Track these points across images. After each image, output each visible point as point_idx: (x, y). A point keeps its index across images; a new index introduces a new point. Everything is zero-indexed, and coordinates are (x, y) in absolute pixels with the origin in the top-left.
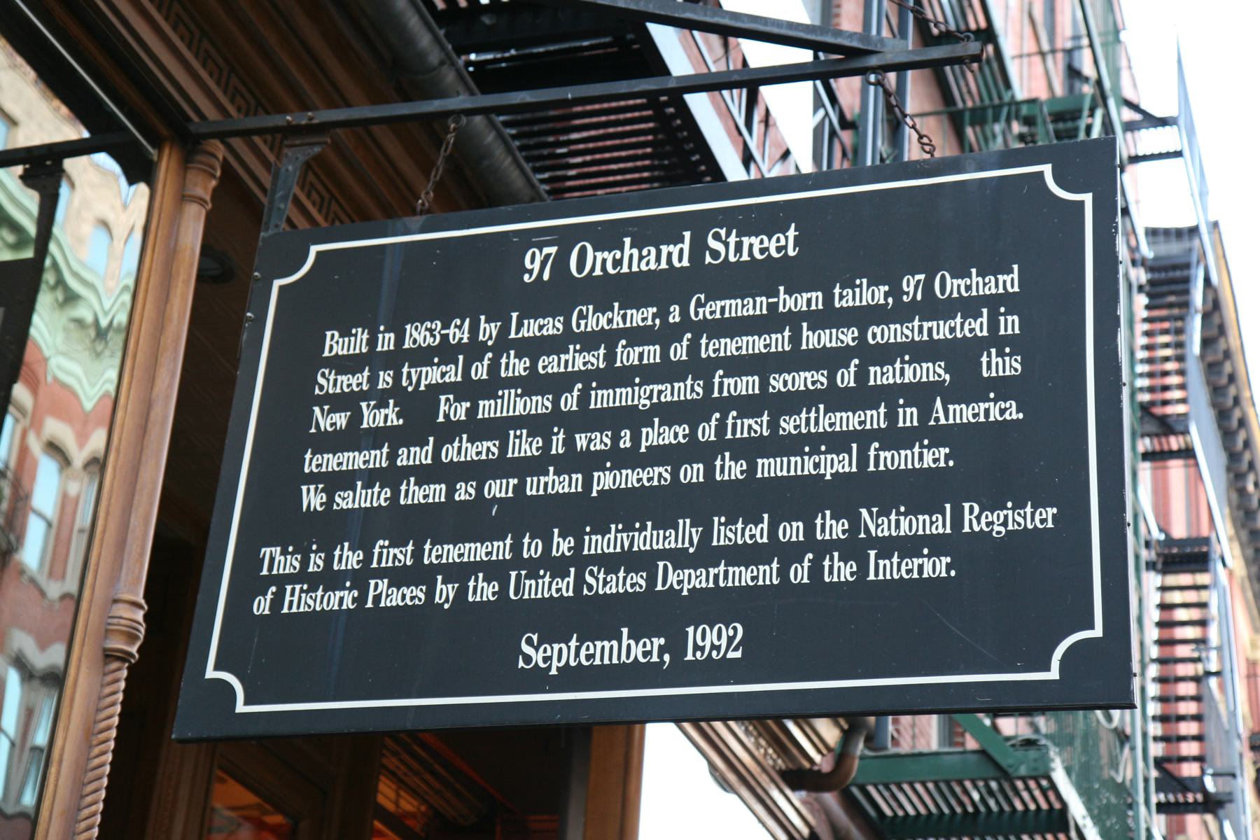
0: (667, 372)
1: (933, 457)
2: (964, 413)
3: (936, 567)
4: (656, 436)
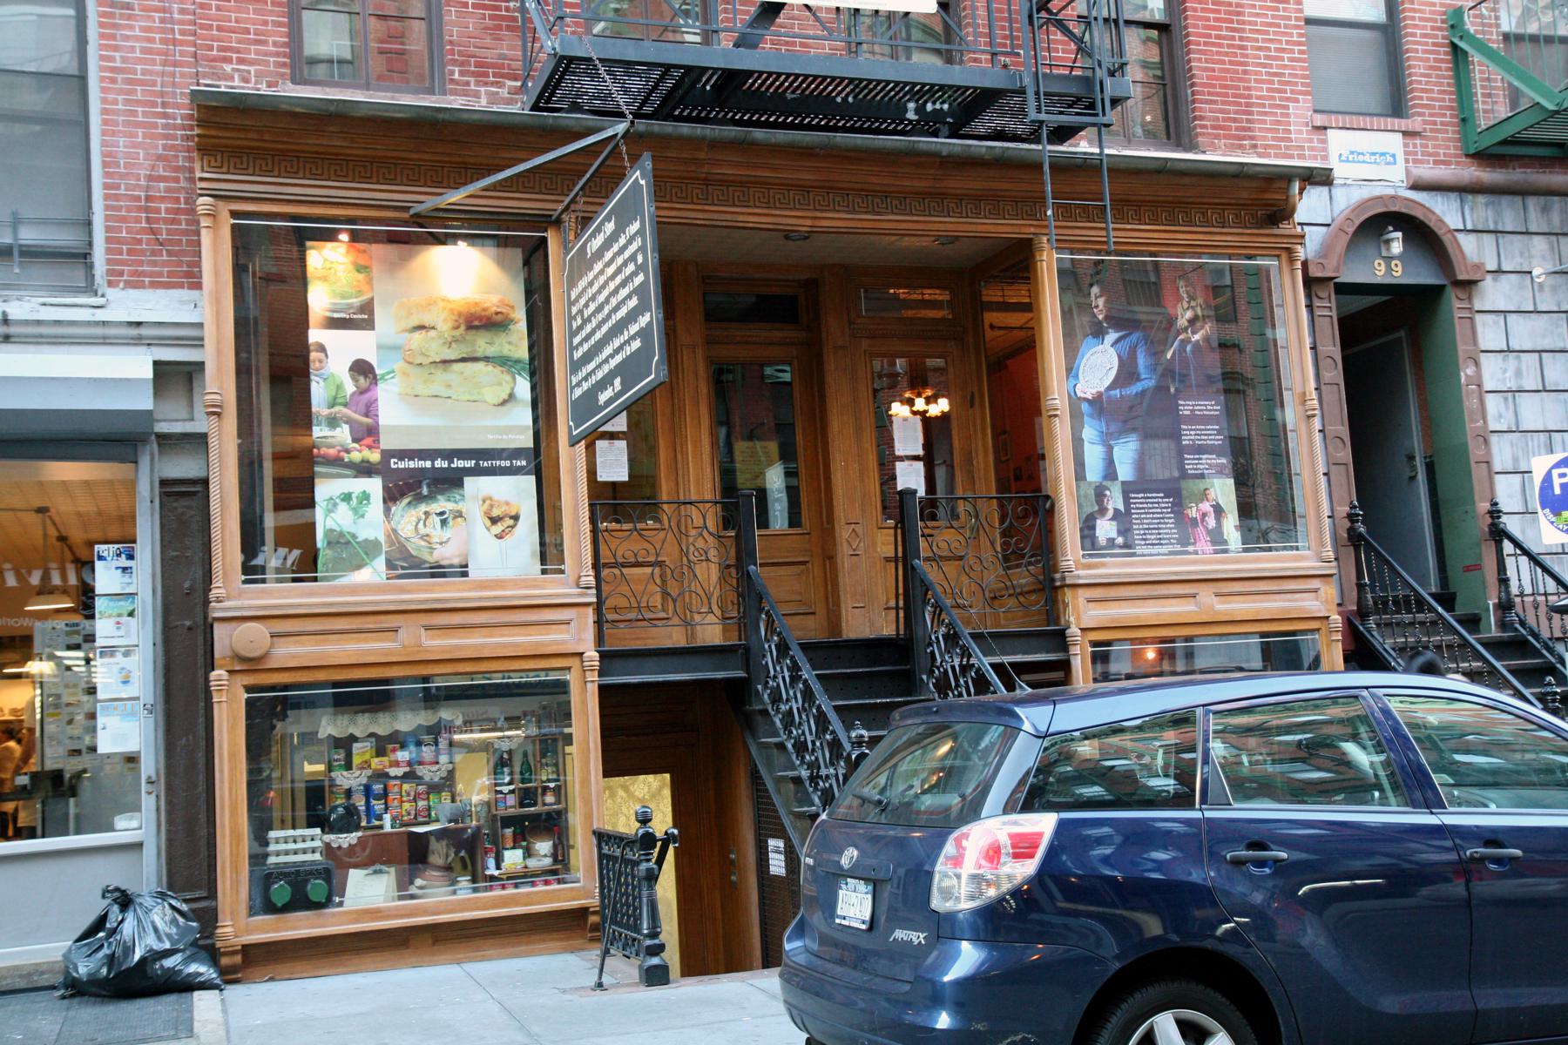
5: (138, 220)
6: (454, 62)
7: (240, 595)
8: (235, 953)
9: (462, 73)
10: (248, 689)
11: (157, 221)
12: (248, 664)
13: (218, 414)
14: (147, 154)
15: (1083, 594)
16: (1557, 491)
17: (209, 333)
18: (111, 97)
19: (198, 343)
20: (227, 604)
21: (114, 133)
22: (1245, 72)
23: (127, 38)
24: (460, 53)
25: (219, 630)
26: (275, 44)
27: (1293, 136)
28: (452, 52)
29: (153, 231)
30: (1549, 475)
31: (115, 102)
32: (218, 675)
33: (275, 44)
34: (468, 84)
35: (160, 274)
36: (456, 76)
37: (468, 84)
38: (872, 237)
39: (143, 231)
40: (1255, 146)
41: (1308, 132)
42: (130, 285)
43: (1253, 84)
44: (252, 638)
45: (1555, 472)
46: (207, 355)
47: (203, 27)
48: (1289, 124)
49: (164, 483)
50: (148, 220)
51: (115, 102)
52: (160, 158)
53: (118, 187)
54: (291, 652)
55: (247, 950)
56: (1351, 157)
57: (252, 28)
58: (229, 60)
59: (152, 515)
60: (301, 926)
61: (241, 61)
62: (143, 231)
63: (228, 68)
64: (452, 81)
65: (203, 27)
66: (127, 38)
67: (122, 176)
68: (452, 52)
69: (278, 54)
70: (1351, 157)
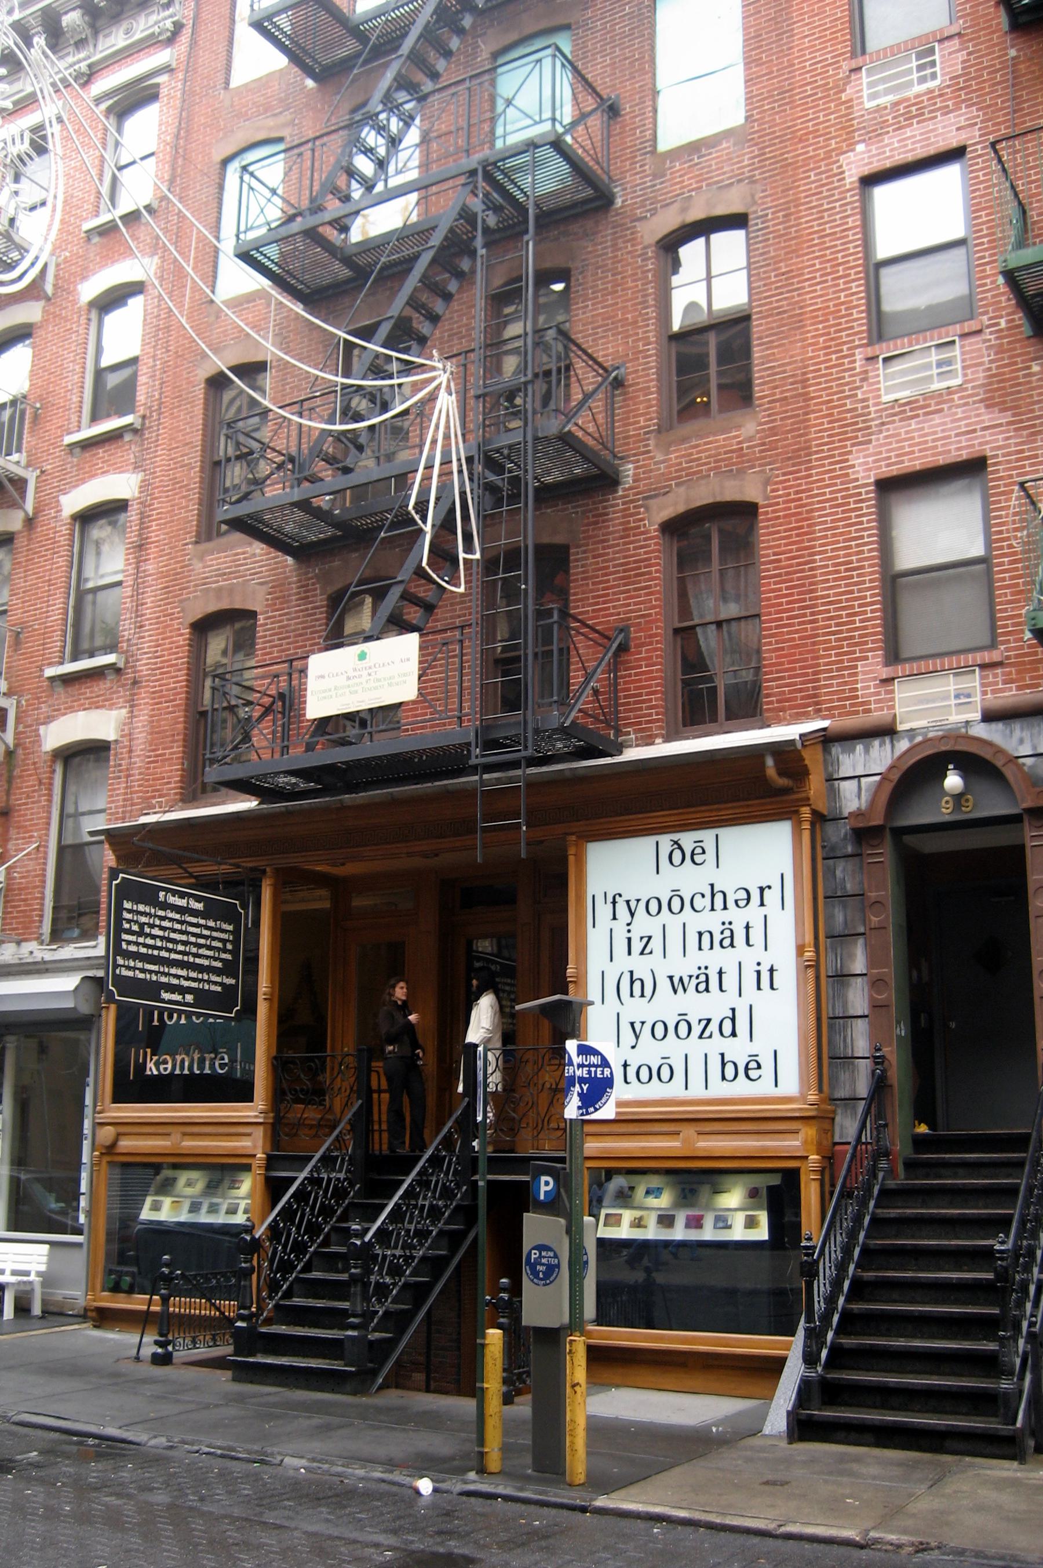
0: (181, 932)
1: (218, 964)
2: (224, 956)
3: (219, 989)
4: (181, 948)
40: (819, 710)
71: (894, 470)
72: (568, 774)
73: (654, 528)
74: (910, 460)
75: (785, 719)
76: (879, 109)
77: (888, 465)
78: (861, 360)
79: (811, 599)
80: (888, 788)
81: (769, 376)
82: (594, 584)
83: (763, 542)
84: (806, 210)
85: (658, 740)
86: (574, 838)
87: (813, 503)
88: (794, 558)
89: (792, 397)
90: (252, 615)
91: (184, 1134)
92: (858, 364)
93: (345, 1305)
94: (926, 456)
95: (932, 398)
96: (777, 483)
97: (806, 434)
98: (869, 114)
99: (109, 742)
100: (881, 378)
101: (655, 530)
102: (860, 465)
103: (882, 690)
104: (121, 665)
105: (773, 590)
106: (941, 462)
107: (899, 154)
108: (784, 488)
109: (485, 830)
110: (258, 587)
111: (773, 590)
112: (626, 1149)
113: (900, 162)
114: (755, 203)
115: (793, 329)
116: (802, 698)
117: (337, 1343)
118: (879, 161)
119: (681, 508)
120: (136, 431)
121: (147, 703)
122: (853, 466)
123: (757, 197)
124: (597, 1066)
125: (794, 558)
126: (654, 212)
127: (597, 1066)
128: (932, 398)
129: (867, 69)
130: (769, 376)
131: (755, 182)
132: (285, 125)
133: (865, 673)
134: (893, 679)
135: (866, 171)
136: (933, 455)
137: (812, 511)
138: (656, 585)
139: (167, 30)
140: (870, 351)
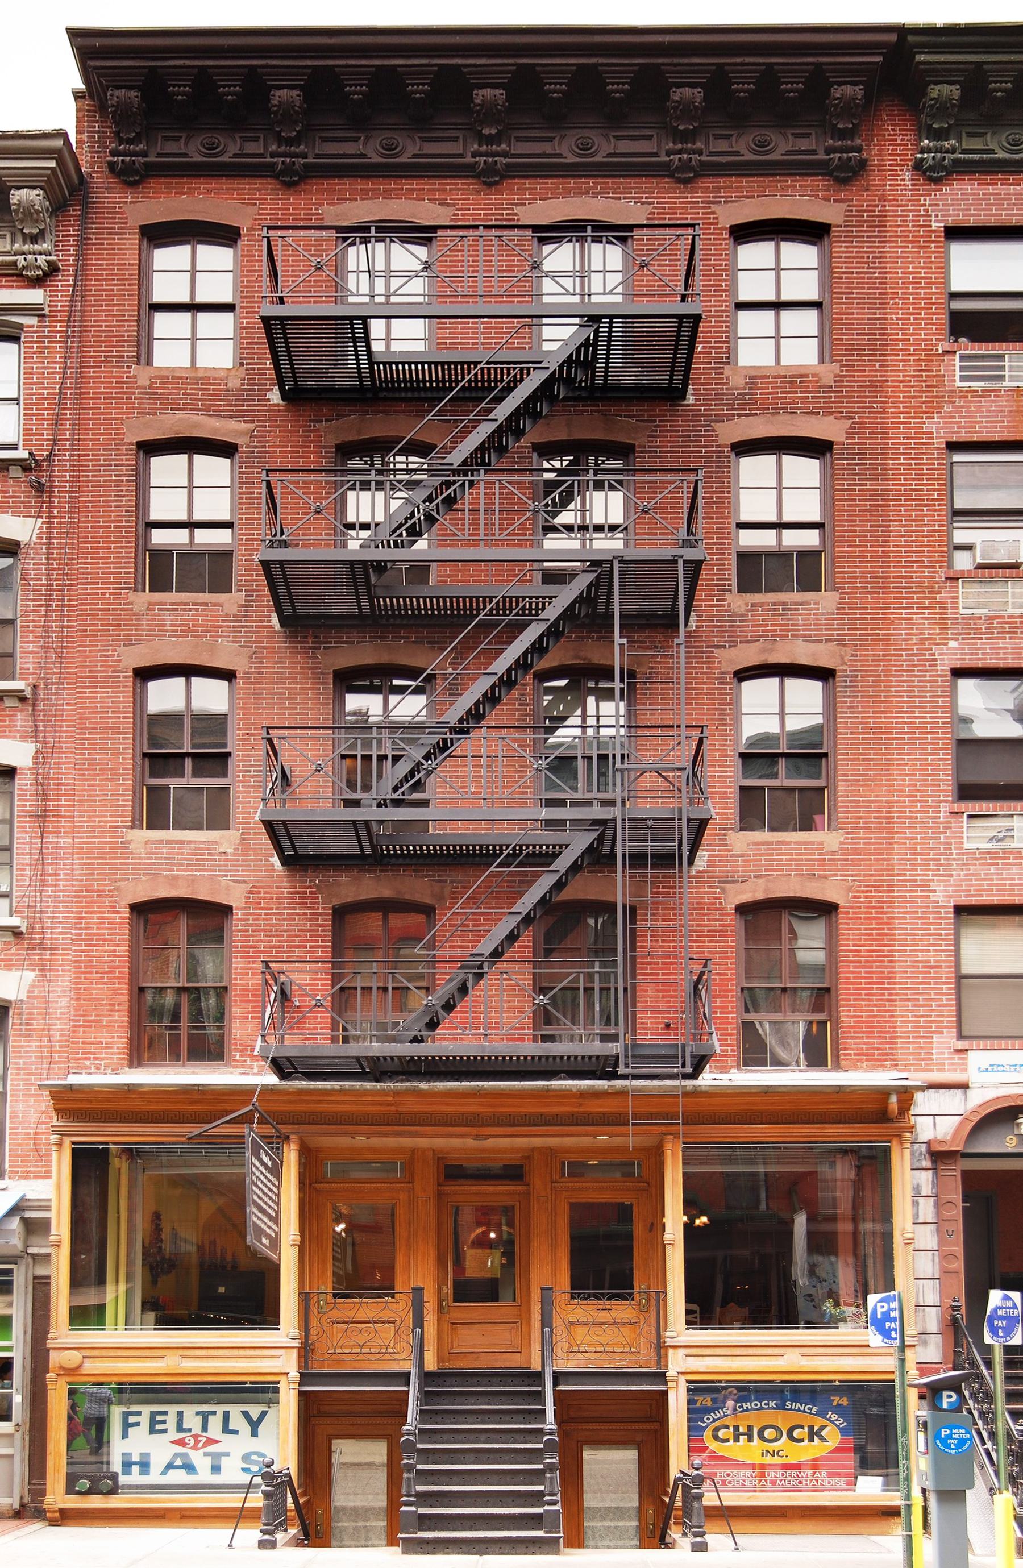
5: (28, 1145)
6: (237, 1050)
7: (67, 1336)
8: (55, 1512)
9: (241, 1056)
10: (70, 1383)
11: (40, 1144)
12: (72, 1371)
13: (58, 1246)
14: (35, 1112)
15: (682, 1352)
16: (879, 1316)
17: (54, 1204)
18: (15, 1082)
19: (48, 1208)
20: (59, 1341)
21: (17, 1101)
22: (892, 1016)
23: (27, 1052)
24: (241, 1045)
25: (53, 1355)
26: (118, 1048)
27: (934, 1057)
28: (236, 1044)
29: (37, 1150)
30: (876, 1306)
31: (19, 1085)
32: (50, 1376)
33: (118, 1048)
34: (245, 1061)
35: (40, 1172)
36: (237, 1058)
37: (245, 1061)
38: (645, 1127)
39: (32, 1150)
40: (896, 1065)
41: (949, 1053)
42: (21, 1178)
43: (899, 1024)
44: (72, 1358)
45: (879, 1305)
46: (52, 1215)
47: (73, 1042)
48: (932, 1048)
49: (35, 1278)
50: (35, 1144)
51: (19, 1085)
52: (43, 1112)
53: (17, 1128)
54: (89, 1367)
55: (62, 1511)
56: (990, 1069)
57: (104, 1040)
58: (88, 1059)
59: (26, 1294)
60: (96, 1502)
61: (96, 1059)
62: (32, 1150)
63: (87, 1063)
64: (234, 1060)
65: (73, 1042)
66: (27, 1052)
67: (20, 1123)
68: (236, 1044)
69: (120, 1053)
70: (990, 1069)
71: (974, 901)
72: (574, 1090)
73: (730, 907)
74: (988, 896)
75: (862, 1067)
76: (972, 617)
77: (966, 896)
78: (945, 812)
79: (889, 983)
80: (970, 1126)
81: (852, 807)
82: (663, 941)
83: (844, 934)
84: (897, 681)
85: (732, 1071)
86: (670, 1137)
87: (894, 913)
88: (873, 951)
89: (875, 828)
90: (229, 909)
91: (183, 1357)
92: (942, 815)
93: (541, 1488)
94: (1004, 895)
95: (1011, 853)
96: (858, 892)
97: (890, 859)
98: (963, 618)
99: (10, 1002)
100: (965, 829)
101: (731, 909)
102: (940, 891)
103: (956, 1057)
104: (23, 929)
105: (853, 972)
106: (1017, 902)
107: (991, 659)
108: (866, 897)
109: (633, 1124)
110: (232, 884)
111: (853, 972)
112: (215, 1368)
113: (991, 666)
114: (844, 663)
115: (880, 775)
116: (879, 1054)
117: (539, 1517)
118: (970, 659)
119: (760, 896)
120: (23, 699)
121: (69, 971)
122: (935, 891)
123: (846, 659)
124: (1010, 1308)
125: (873, 951)
126: (734, 644)
127: (1010, 1308)
128: (1011, 853)
129: (963, 582)
130: (852, 807)
131: (844, 645)
132: (242, 433)
133: (938, 1043)
134: (967, 1050)
135: (958, 664)
136: (1010, 895)
137: (893, 918)
138: (732, 952)
139: (39, 267)
140: (956, 807)
